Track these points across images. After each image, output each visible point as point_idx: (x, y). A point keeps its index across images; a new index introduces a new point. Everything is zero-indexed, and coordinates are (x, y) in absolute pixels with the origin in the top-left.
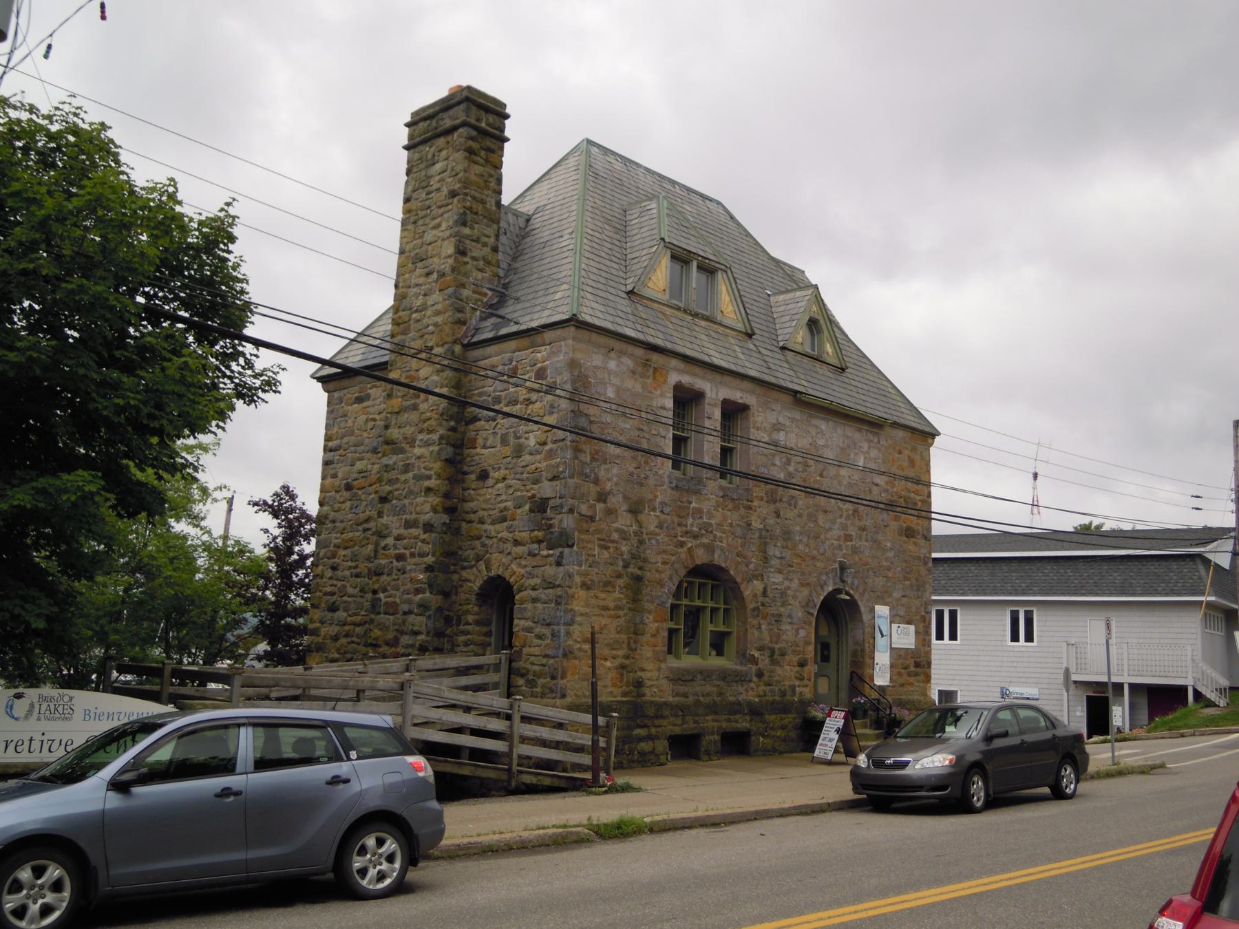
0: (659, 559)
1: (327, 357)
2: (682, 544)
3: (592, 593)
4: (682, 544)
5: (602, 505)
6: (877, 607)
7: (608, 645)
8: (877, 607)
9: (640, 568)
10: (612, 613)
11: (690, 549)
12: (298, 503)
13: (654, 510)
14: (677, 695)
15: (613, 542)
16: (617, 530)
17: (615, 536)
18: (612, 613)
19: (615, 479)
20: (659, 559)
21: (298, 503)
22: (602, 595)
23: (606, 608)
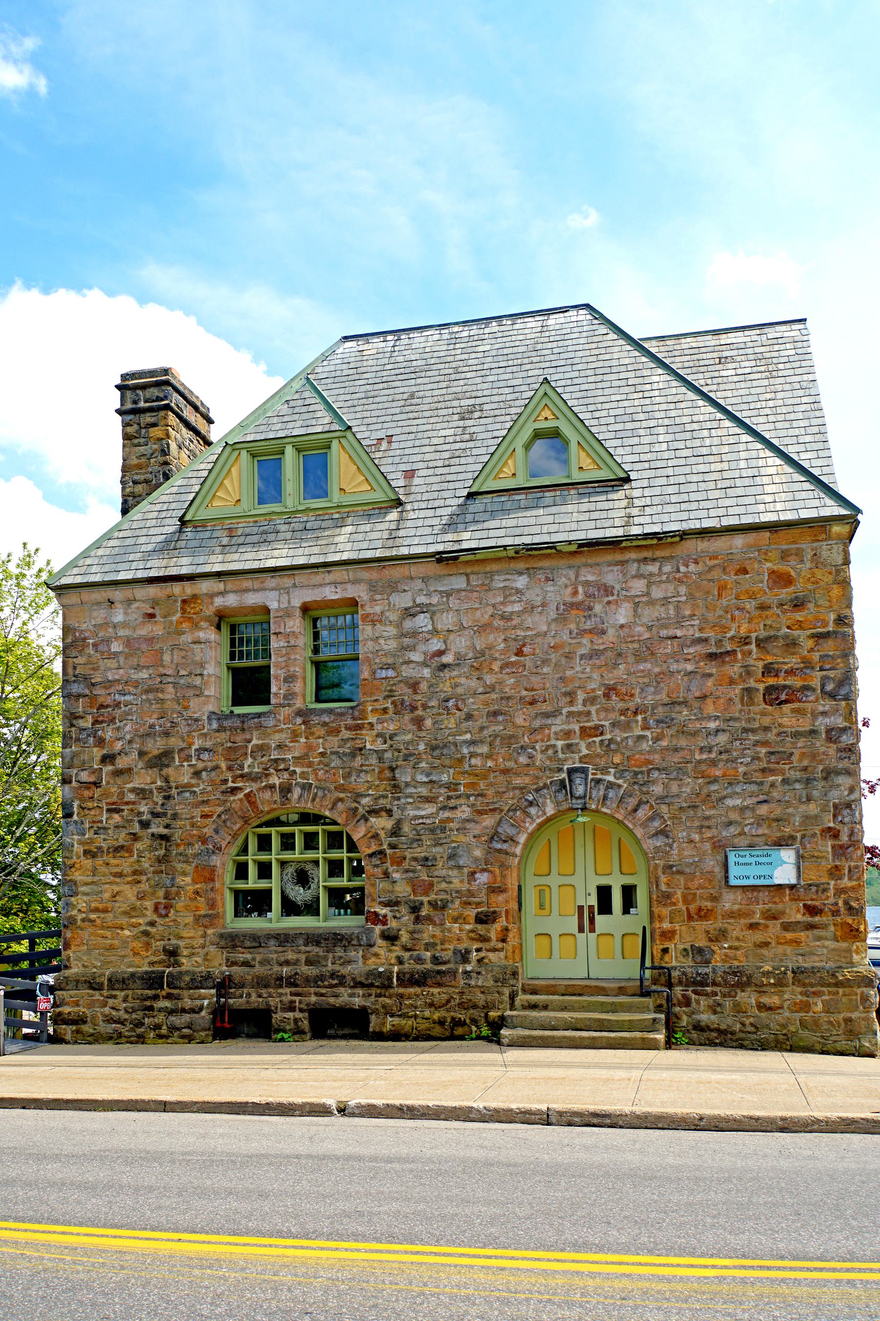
0: (197, 812)
1: (636, 337)
2: (234, 791)
3: (99, 861)
4: (234, 791)
5: (110, 768)
6: (788, 855)
7: (125, 913)
8: (788, 855)
9: (167, 826)
10: (129, 879)
11: (247, 796)
12: (35, 558)
13: (188, 758)
14: (234, 963)
15: (127, 803)
16: (133, 790)
17: (131, 797)
18: (129, 879)
19: (128, 737)
20: (197, 812)
21: (35, 558)
22: (113, 861)
23: (120, 875)
